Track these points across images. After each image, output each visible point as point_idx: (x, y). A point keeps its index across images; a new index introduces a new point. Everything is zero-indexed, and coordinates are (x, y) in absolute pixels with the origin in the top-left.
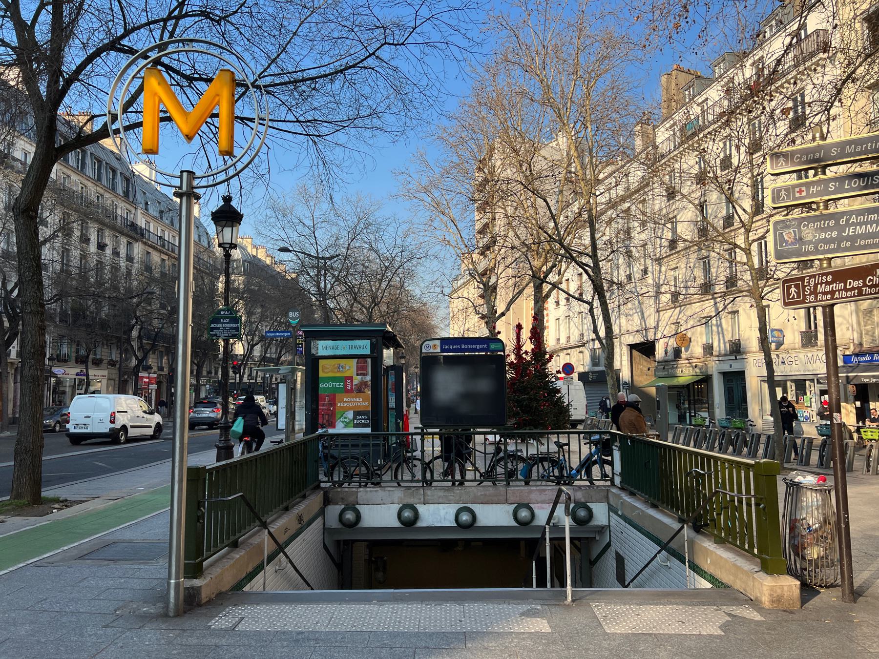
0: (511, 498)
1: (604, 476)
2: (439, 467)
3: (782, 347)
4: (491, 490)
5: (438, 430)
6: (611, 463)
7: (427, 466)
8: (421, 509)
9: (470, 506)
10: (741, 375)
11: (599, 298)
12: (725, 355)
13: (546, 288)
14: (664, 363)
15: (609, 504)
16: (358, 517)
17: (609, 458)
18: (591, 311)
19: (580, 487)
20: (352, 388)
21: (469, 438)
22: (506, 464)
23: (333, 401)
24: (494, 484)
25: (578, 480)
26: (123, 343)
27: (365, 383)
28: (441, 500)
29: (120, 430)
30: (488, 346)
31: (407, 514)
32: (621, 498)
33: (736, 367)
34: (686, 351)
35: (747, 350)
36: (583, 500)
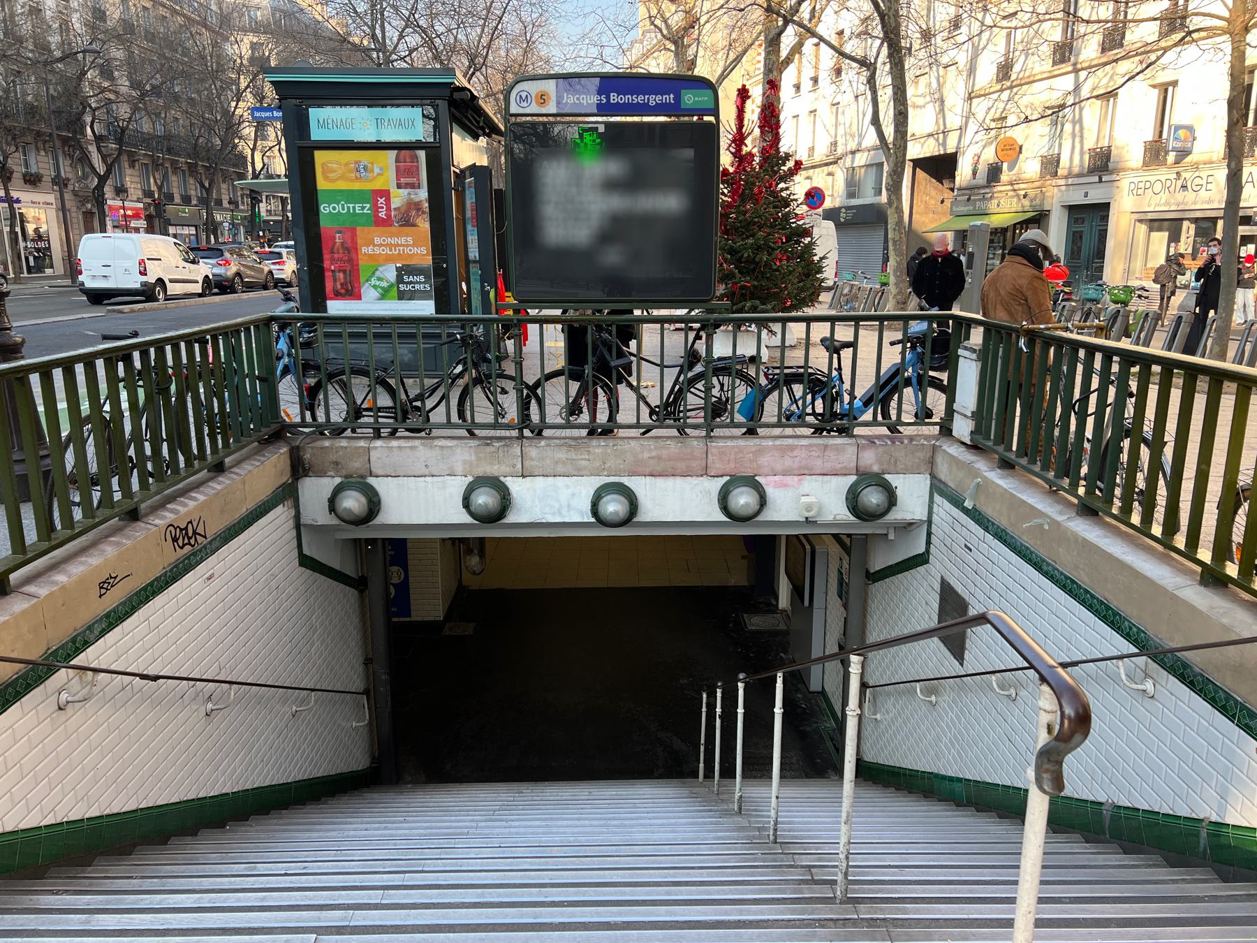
0: (717, 465)
1: (924, 414)
2: (557, 395)
3: (1188, 159)
4: (673, 448)
5: (558, 312)
6: (949, 390)
7: (531, 394)
8: (517, 487)
9: (626, 481)
10: (1102, 210)
11: (890, 56)
12: (1080, 175)
13: (789, 38)
14: (970, 189)
15: (933, 477)
16: (374, 504)
17: (944, 376)
18: (871, 81)
19: (871, 440)
20: (388, 215)
21: (628, 332)
22: (708, 389)
23: (351, 249)
24: (681, 431)
25: (866, 424)
26: (71, 144)
27: (417, 206)
28: (560, 469)
29: (155, 285)
30: (678, 99)
31: (484, 499)
32: (976, 473)
33: (1096, 196)
34: (1011, 168)
35: (1121, 165)
36: (876, 469)
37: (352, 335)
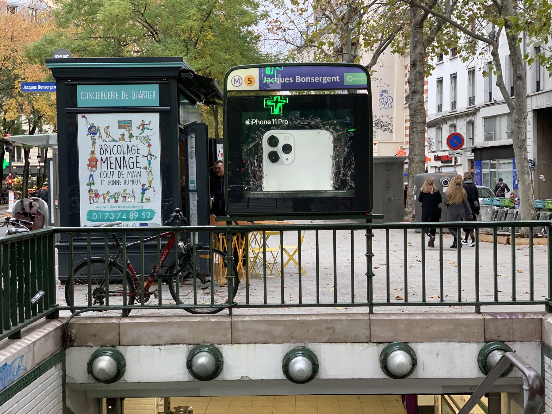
8: (229, 352)
30: (342, 79)
37: (94, 247)
